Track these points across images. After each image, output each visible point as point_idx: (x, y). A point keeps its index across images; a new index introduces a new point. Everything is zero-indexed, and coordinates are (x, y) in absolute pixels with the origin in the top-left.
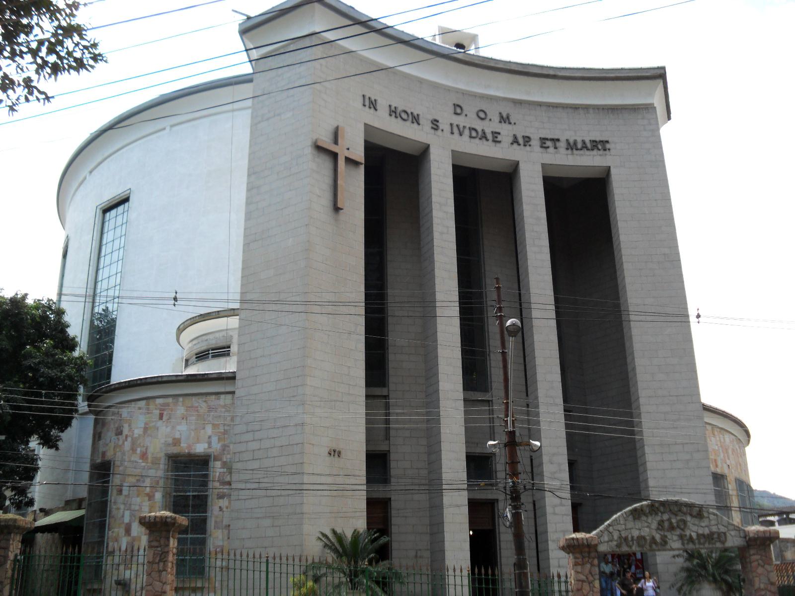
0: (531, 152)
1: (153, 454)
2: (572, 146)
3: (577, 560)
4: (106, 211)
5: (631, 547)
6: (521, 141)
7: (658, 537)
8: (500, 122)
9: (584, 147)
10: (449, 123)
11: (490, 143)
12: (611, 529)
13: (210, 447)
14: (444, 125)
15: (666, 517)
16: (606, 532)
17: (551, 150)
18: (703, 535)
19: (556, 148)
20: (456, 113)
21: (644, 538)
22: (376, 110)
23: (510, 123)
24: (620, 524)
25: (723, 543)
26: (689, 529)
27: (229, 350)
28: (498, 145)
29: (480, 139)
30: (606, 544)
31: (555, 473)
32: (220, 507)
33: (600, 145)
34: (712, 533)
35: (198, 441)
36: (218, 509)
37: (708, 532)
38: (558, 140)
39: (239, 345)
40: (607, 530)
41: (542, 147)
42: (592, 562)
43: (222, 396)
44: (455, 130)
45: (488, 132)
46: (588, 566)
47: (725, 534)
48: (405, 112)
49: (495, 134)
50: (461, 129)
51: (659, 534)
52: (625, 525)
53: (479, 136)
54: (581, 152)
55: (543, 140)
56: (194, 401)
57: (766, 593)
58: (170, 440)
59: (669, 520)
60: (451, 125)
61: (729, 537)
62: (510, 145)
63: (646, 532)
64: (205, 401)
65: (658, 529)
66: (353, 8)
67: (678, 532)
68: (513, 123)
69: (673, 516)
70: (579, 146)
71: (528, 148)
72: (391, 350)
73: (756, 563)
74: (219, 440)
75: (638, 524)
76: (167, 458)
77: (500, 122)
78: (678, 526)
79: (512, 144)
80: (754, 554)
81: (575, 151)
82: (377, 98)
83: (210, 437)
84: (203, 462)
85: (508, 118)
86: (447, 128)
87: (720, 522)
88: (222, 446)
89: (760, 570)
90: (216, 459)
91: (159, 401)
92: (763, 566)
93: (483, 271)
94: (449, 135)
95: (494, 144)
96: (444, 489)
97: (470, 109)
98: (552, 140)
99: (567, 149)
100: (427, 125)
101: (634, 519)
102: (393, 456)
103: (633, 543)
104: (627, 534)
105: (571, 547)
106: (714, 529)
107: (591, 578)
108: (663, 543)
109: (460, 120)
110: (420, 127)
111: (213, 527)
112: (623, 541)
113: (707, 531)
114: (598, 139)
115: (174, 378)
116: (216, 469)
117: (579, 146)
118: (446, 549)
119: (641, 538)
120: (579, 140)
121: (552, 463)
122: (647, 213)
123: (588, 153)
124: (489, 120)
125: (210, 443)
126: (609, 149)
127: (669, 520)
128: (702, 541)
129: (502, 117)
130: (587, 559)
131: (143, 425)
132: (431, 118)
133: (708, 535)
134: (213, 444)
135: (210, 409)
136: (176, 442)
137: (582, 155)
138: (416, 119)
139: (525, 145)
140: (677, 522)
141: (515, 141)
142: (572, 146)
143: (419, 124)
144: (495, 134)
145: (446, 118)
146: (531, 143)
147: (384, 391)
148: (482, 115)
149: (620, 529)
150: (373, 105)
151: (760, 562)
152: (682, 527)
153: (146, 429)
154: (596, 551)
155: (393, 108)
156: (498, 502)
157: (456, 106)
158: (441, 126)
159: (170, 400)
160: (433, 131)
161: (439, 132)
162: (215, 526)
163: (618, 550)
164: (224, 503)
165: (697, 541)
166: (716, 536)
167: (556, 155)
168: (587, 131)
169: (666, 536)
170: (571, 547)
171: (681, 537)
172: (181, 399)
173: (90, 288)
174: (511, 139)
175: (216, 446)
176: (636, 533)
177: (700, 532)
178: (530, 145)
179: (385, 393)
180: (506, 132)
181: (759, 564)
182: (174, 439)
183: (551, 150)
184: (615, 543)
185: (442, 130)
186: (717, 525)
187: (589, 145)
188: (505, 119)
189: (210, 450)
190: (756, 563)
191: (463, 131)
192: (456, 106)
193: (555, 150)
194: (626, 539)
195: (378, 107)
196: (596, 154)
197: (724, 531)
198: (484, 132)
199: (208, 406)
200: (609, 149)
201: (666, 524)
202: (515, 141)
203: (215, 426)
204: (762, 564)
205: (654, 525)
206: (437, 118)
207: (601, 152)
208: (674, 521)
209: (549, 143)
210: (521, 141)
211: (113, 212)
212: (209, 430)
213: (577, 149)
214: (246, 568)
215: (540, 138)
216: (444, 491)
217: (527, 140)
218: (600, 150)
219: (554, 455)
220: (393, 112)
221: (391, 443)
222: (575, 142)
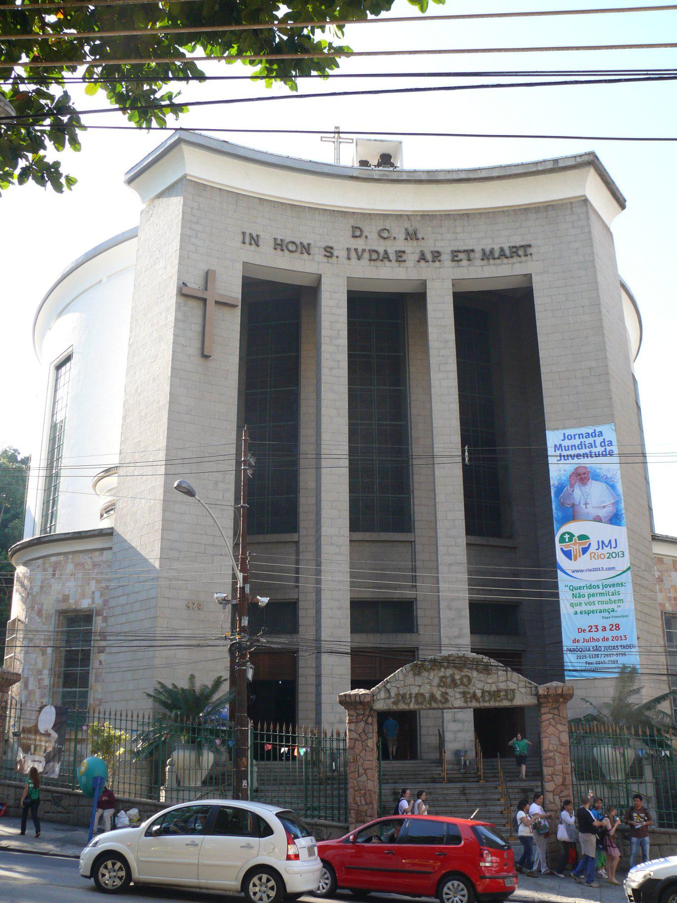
0: (440, 268)
1: (47, 610)
2: (488, 256)
3: (352, 718)
4: (59, 367)
5: (408, 704)
6: (429, 257)
7: (438, 695)
8: (406, 239)
10: (345, 249)
12: (388, 686)
13: (93, 603)
15: (449, 672)
16: (383, 689)
17: (465, 263)
18: (489, 692)
19: (469, 260)
20: (354, 237)
21: (422, 695)
22: (258, 246)
23: (417, 239)
24: (399, 680)
25: (512, 700)
28: (402, 264)
29: (382, 261)
30: (382, 701)
31: (453, 619)
32: (100, 661)
33: (520, 251)
34: (499, 691)
35: (83, 596)
36: (98, 663)
37: (496, 689)
38: (473, 251)
40: (385, 686)
41: (453, 261)
42: (367, 720)
43: (105, 552)
44: (353, 255)
45: (391, 251)
46: (362, 724)
47: (513, 690)
48: (294, 243)
49: (400, 254)
50: (360, 253)
52: (404, 681)
53: (381, 258)
54: (498, 261)
55: (455, 254)
56: (82, 558)
57: (555, 754)
58: (61, 597)
59: (452, 676)
60: (348, 250)
61: (518, 695)
62: (416, 263)
63: (426, 690)
64: (91, 558)
65: (439, 686)
66: (227, 142)
67: (461, 689)
68: (421, 239)
69: (456, 672)
70: (497, 255)
71: (437, 264)
72: (302, 493)
73: (547, 722)
74: (102, 595)
75: (419, 680)
76: (57, 614)
77: (406, 239)
78: (462, 683)
79: (418, 261)
80: (546, 713)
81: (492, 261)
82: (259, 233)
83: (93, 593)
84: (87, 617)
85: (415, 233)
86: (343, 254)
87: (509, 678)
88: (103, 601)
89: (551, 730)
90: (98, 614)
91: (53, 559)
92: (554, 727)
93: (409, 401)
95: (397, 264)
97: (371, 230)
98: (465, 251)
99: (483, 259)
100: (318, 254)
101: (415, 675)
102: (301, 605)
103: (411, 701)
104: (405, 692)
105: (347, 702)
106: (502, 686)
107: (364, 737)
108: (443, 701)
109: (360, 244)
110: (311, 256)
111: (93, 681)
112: (400, 698)
113: (494, 688)
114: (518, 244)
115: (63, 537)
116: (98, 624)
117: (497, 255)
118: (323, 701)
119: (419, 695)
122: (572, 322)
123: (505, 261)
125: (93, 599)
126: (531, 254)
127: (452, 676)
128: (487, 699)
129: (408, 234)
130: (361, 717)
132: (324, 245)
133: (494, 691)
134: (96, 599)
135: (95, 565)
136: (66, 598)
137: (500, 265)
138: (306, 249)
139: (434, 261)
140: (461, 679)
141: (423, 257)
142: (488, 256)
143: (309, 254)
144: (400, 254)
145: (342, 241)
147: (295, 537)
149: (398, 686)
150: (255, 240)
151: (552, 721)
152: (466, 683)
153: (42, 587)
154: (371, 709)
155: (279, 242)
156: (418, 650)
157: (355, 228)
158: (336, 253)
159: (62, 558)
160: (325, 259)
162: (95, 680)
163: (395, 707)
164: (102, 657)
165: (481, 700)
166: (502, 693)
167: (471, 268)
168: (506, 238)
169: (446, 693)
170: (347, 702)
171: (464, 694)
172: (70, 556)
175: (99, 601)
176: (415, 690)
177: (487, 688)
178: (440, 261)
179: (296, 539)
182: (64, 596)
183: (465, 263)
184: (392, 700)
185: (337, 257)
186: (506, 681)
187: (507, 253)
189: (94, 606)
190: (547, 722)
191: (362, 254)
192: (355, 228)
193: (469, 262)
194: (404, 696)
195: (260, 243)
197: (513, 688)
198: (386, 252)
199: (93, 562)
200: (531, 254)
201: (449, 680)
203: (98, 581)
204: (554, 723)
205: (436, 681)
206: (330, 245)
207: (523, 258)
208: (457, 677)
209: (461, 256)
210: (429, 257)
211: (63, 369)
212: (93, 585)
213: (494, 259)
215: (452, 251)
217: (437, 255)
218: (520, 256)
219: (453, 600)
220: (280, 245)
221: (300, 591)
222: (492, 251)
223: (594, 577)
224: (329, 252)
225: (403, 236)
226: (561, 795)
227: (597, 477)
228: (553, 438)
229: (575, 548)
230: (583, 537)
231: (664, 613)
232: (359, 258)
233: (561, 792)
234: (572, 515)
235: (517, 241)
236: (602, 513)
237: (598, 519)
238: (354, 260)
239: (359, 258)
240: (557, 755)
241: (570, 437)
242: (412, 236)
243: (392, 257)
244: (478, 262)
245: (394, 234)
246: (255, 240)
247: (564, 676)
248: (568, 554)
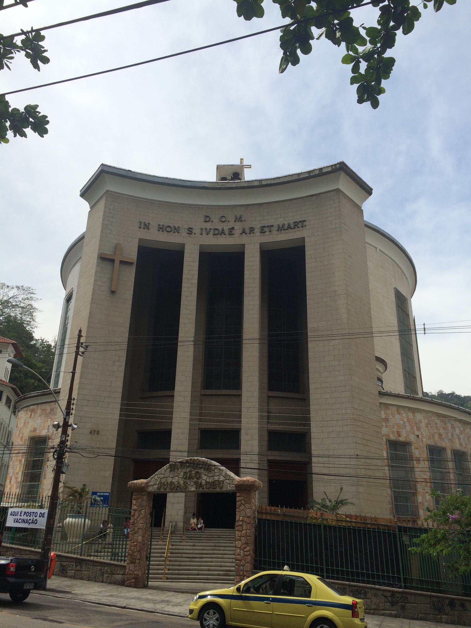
2: (281, 228)
6: (248, 231)
7: (182, 482)
9: (289, 227)
11: (227, 236)
14: (197, 231)
15: (188, 470)
17: (267, 233)
18: (209, 482)
26: (202, 478)
38: (272, 226)
44: (204, 232)
51: (192, 482)
58: (32, 429)
60: (202, 229)
69: (193, 470)
71: (252, 235)
81: (283, 231)
83: (49, 426)
92: (244, 505)
94: (199, 236)
96: (257, 455)
100: (184, 233)
110: (179, 234)
120: (286, 223)
121: (247, 434)
131: (23, 421)
132: (187, 227)
138: (177, 230)
141: (244, 232)
142: (281, 228)
146: (254, 231)
148: (223, 219)
150: (147, 226)
158: (194, 232)
160: (188, 235)
161: (193, 235)
174: (241, 231)
176: (169, 480)
178: (253, 233)
180: (238, 227)
181: (241, 503)
188: (239, 219)
196: (296, 230)
202: (244, 232)
206: (191, 227)
207: (301, 228)
214: (14, 497)
216: (257, 454)
217: (252, 230)
220: (161, 228)
224: (190, 231)
226: (244, 550)
233: (245, 548)
235: (298, 219)
238: (204, 235)
240: (244, 523)
246: (147, 226)
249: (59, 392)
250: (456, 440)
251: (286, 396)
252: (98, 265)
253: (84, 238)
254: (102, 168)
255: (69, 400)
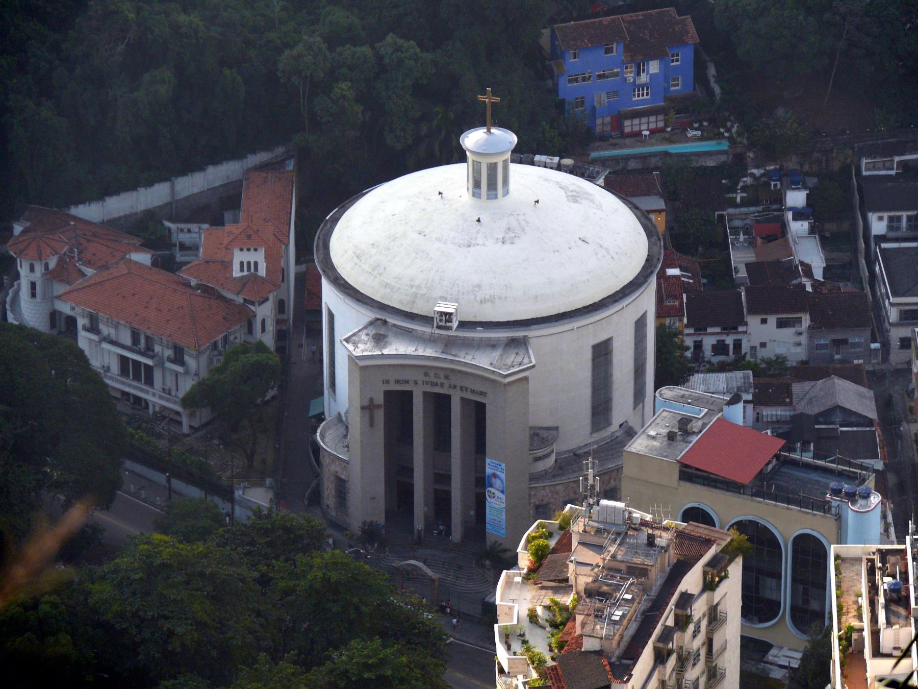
9: (477, 393)
27: (530, 450)
33: (483, 394)
39: (109, 351)
44: (425, 383)
60: (423, 382)
97: (432, 374)
100: (412, 383)
109: (427, 379)
124: (419, 382)
138: (407, 382)
141: (450, 386)
142: (473, 392)
145: (420, 378)
150: (388, 382)
158: (418, 382)
168: (478, 387)
173: (776, 411)
183: (464, 391)
192: (425, 373)
217: (455, 387)
220: (397, 382)
223: (496, 506)
224: (416, 382)
225: (443, 377)
227: (499, 478)
228: (488, 461)
229: (492, 496)
230: (493, 493)
231: (769, 646)
232: (427, 384)
234: (491, 486)
235: (483, 389)
236: (499, 489)
237: (498, 490)
238: (425, 385)
239: (427, 384)
241: (493, 463)
242: (447, 377)
243: (439, 384)
244: (469, 393)
245: (440, 376)
246: (388, 382)
247: (802, 659)
248: (489, 496)
249: (530, 479)
250: (172, 429)
251: (822, 537)
252: (361, 412)
253: (725, 648)
254: (658, 676)
255: (802, 464)
